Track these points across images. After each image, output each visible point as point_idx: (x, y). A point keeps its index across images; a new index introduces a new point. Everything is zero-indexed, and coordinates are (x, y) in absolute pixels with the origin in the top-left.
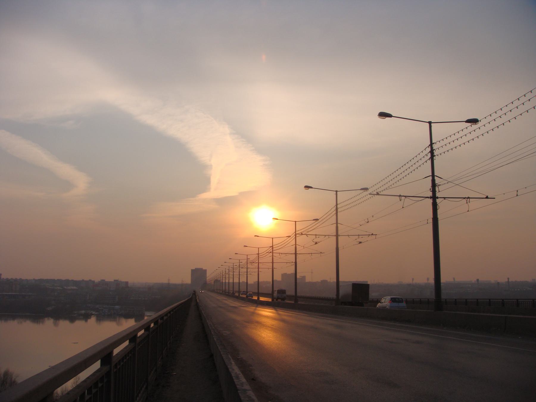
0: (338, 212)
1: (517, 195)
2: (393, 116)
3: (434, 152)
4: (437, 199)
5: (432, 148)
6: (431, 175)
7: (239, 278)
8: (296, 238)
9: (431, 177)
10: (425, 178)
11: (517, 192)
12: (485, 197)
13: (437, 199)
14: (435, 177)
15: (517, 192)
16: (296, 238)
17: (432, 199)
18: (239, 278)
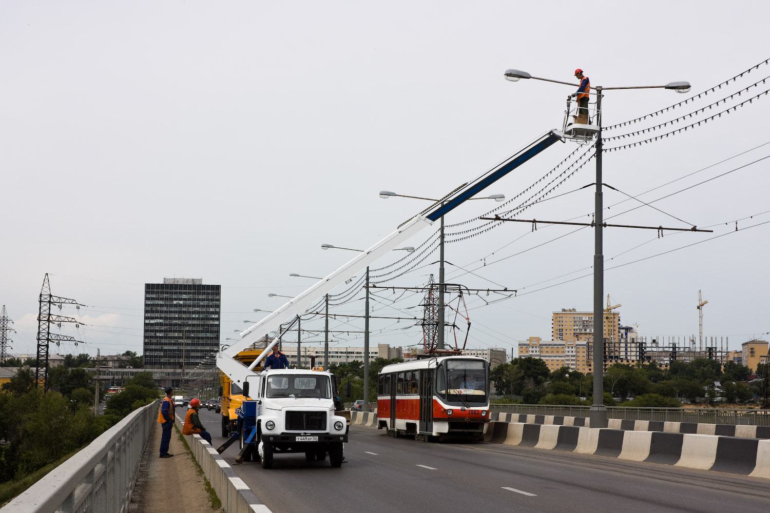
0: (602, 150)
1: (737, 228)
2: (532, 76)
3: (603, 142)
4: (603, 227)
5: (442, 232)
6: (440, 260)
7: (367, 333)
8: (442, 244)
9: (595, 186)
10: (584, 187)
11: (736, 223)
12: (690, 227)
13: (603, 227)
14: (444, 262)
15: (736, 223)
16: (442, 244)
17: (594, 227)
18: (367, 333)
